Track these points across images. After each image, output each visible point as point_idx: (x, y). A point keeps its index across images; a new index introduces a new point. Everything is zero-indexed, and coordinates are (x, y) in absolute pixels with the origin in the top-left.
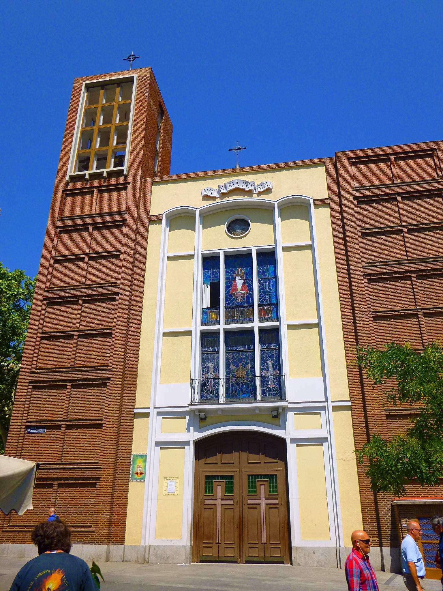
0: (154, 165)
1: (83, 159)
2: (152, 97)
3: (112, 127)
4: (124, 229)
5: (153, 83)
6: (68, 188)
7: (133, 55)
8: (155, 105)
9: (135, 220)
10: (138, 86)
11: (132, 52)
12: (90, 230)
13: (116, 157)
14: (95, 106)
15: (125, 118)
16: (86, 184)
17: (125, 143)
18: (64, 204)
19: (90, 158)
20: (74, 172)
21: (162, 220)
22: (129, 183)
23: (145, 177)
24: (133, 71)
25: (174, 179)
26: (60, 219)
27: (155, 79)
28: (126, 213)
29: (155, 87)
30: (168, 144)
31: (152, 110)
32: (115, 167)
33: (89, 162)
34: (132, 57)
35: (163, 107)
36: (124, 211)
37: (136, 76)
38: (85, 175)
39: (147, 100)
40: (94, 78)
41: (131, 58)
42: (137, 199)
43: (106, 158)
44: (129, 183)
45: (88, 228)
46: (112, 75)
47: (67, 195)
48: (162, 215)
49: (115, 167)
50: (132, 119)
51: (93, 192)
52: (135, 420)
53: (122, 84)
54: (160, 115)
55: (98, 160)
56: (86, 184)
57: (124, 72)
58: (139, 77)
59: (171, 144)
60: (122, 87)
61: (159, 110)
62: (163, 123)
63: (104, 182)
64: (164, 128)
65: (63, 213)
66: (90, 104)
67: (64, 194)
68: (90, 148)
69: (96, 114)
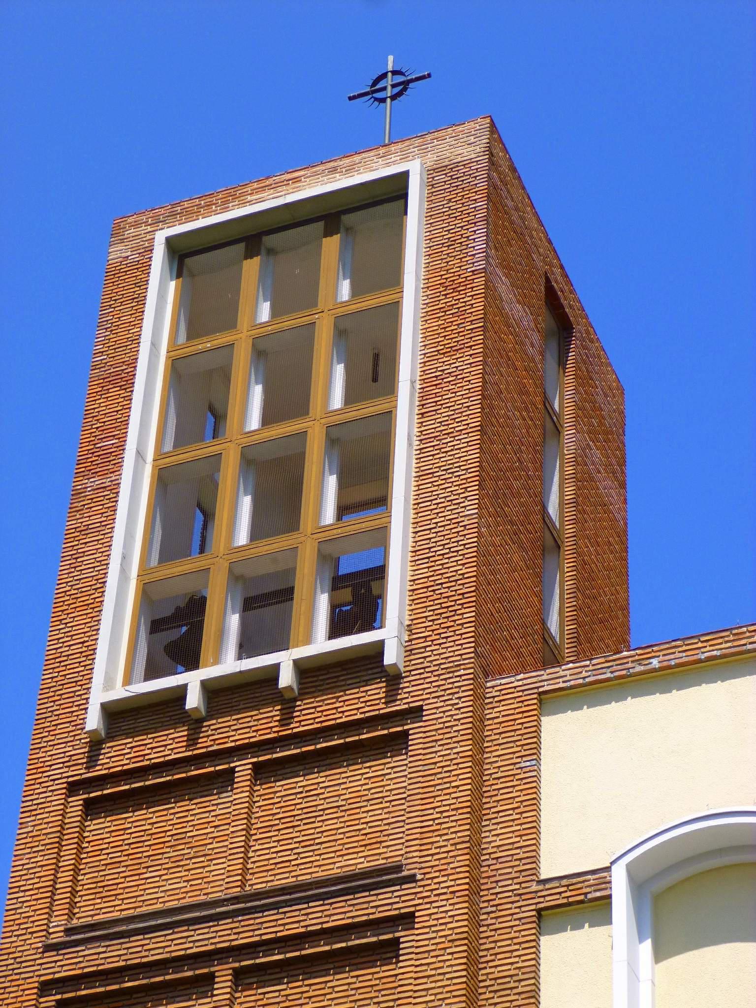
0: (541, 601)
1: (168, 612)
2: (507, 267)
3: (310, 431)
4: (406, 966)
5: (504, 194)
6: (99, 771)
7: (394, 73)
8: (524, 300)
9: (462, 908)
10: (430, 216)
11: (391, 58)
12: (223, 986)
13: (337, 583)
14: (222, 339)
15: (375, 379)
16: (192, 741)
17: (382, 501)
18: (79, 859)
19: (203, 601)
20: (128, 680)
21: (610, 897)
22: (415, 713)
23: (501, 672)
24: (400, 146)
25: (654, 670)
26: (58, 937)
27: (514, 170)
28: (412, 879)
29: (517, 209)
30: (605, 484)
31: (508, 326)
32: (335, 632)
33: (202, 622)
34: (390, 80)
35: (565, 303)
36: (398, 868)
37: (415, 169)
38: (181, 692)
39: (480, 281)
40: (209, 206)
41: (385, 89)
42: (464, 795)
43: (286, 594)
44: (415, 713)
45: (210, 979)
46: (296, 180)
47: (92, 809)
48: (608, 869)
49: (335, 632)
50: (413, 382)
51: (226, 779)
52: (545, 720)
53: (346, 219)
54: (554, 345)
55: (249, 605)
56: (192, 741)
57: (357, 158)
58: (432, 172)
59: (623, 485)
60: (348, 230)
61: (546, 320)
62: (569, 380)
63: (286, 718)
64: (579, 407)
65: (72, 905)
66: (192, 335)
67: (77, 802)
68: (202, 550)
69: (228, 380)
